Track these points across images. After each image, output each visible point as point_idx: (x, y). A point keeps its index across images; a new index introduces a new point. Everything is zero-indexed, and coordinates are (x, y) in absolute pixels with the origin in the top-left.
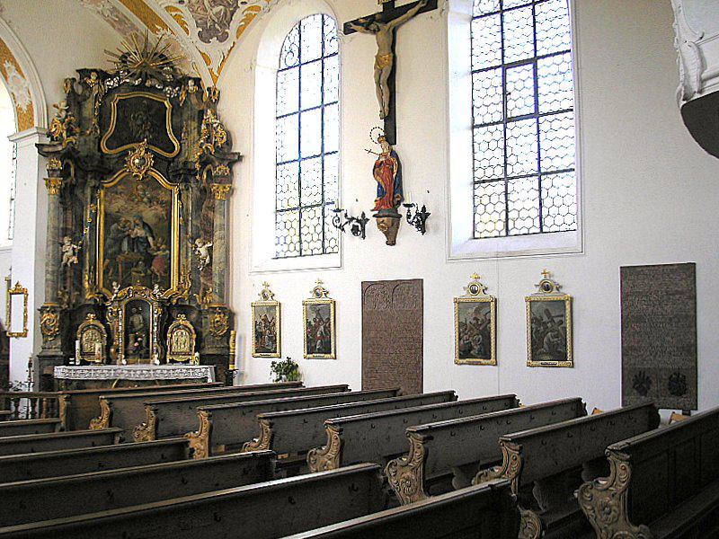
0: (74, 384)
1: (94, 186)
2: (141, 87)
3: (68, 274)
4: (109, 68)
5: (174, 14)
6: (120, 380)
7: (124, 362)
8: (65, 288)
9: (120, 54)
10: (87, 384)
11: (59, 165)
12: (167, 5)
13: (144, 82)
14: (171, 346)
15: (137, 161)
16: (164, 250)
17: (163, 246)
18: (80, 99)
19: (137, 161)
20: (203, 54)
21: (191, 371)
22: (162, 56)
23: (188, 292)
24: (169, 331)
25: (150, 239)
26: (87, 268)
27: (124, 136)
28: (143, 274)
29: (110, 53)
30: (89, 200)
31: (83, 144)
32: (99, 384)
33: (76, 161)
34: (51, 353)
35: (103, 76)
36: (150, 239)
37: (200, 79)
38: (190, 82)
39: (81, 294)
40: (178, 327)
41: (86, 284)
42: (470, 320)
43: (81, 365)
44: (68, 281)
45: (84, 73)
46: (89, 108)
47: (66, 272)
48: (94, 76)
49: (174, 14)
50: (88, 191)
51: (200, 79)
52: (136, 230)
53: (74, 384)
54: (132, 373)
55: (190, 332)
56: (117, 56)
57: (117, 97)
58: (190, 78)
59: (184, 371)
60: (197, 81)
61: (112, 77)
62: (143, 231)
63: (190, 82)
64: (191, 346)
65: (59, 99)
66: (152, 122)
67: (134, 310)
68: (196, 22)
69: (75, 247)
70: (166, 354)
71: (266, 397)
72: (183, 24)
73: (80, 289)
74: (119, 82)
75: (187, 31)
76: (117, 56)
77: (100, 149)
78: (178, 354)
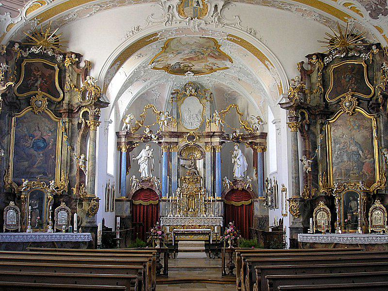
0: (308, 245)
1: (322, 123)
2: (346, 58)
3: (309, 178)
4: (324, 50)
5: (350, 7)
6: (336, 244)
7: (340, 232)
8: (307, 187)
9: (329, 41)
10: (316, 245)
11: (294, 114)
12: (343, 3)
13: (347, 54)
14: (371, 222)
15: (347, 104)
16: (370, 158)
17: (369, 156)
18: (308, 73)
19: (347, 104)
20: (376, 27)
21: (379, 238)
22: (352, 35)
23: (385, 185)
24: (370, 211)
25: (360, 152)
26: (320, 174)
27: (340, 90)
28: (357, 175)
29: (321, 42)
30: (319, 132)
31: (313, 100)
32: (324, 245)
33: (308, 109)
34: (296, 226)
35: (321, 56)
36: (360, 152)
37: (380, 44)
38: (374, 47)
39: (318, 190)
40: (376, 208)
41: (320, 184)
42: (127, 213)
43: (316, 233)
44: (309, 181)
45: (309, 57)
46: (315, 77)
47: (307, 177)
48: (314, 58)
49: (350, 7)
50: (318, 127)
51: (380, 44)
52: (351, 147)
53: (308, 245)
54: (341, 239)
55: (384, 212)
56: (327, 43)
57: (333, 67)
58: (373, 45)
59: (374, 238)
60: (378, 45)
61: (327, 56)
62: (356, 148)
63: (374, 47)
64: (384, 221)
65: (296, 75)
66: (355, 78)
67: (351, 198)
68: (366, 8)
69: (310, 161)
70: (368, 226)
71: (55, 269)
72: (357, 11)
73: (317, 187)
74: (332, 58)
75: (362, 15)
76: (327, 43)
77: (325, 100)
78: (376, 227)
